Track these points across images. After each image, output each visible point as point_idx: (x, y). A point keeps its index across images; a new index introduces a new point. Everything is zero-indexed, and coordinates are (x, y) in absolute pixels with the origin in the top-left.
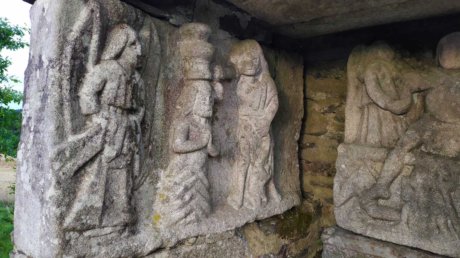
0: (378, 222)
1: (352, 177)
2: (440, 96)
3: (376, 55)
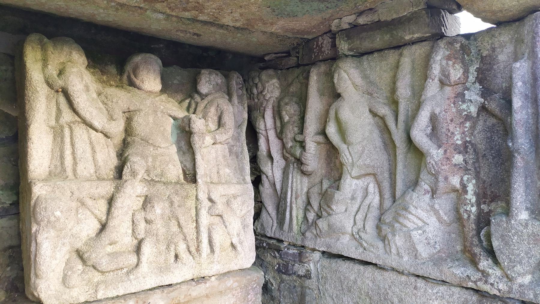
0: (108, 276)
1: (70, 227)
2: (150, 119)
3: (68, 56)
